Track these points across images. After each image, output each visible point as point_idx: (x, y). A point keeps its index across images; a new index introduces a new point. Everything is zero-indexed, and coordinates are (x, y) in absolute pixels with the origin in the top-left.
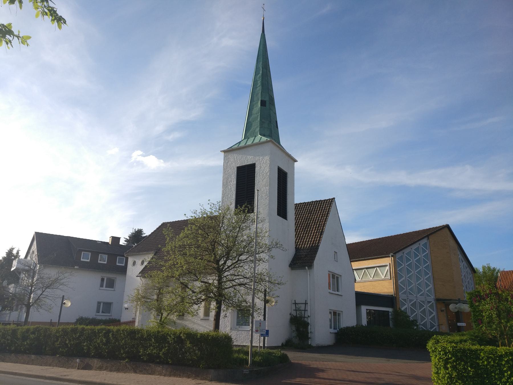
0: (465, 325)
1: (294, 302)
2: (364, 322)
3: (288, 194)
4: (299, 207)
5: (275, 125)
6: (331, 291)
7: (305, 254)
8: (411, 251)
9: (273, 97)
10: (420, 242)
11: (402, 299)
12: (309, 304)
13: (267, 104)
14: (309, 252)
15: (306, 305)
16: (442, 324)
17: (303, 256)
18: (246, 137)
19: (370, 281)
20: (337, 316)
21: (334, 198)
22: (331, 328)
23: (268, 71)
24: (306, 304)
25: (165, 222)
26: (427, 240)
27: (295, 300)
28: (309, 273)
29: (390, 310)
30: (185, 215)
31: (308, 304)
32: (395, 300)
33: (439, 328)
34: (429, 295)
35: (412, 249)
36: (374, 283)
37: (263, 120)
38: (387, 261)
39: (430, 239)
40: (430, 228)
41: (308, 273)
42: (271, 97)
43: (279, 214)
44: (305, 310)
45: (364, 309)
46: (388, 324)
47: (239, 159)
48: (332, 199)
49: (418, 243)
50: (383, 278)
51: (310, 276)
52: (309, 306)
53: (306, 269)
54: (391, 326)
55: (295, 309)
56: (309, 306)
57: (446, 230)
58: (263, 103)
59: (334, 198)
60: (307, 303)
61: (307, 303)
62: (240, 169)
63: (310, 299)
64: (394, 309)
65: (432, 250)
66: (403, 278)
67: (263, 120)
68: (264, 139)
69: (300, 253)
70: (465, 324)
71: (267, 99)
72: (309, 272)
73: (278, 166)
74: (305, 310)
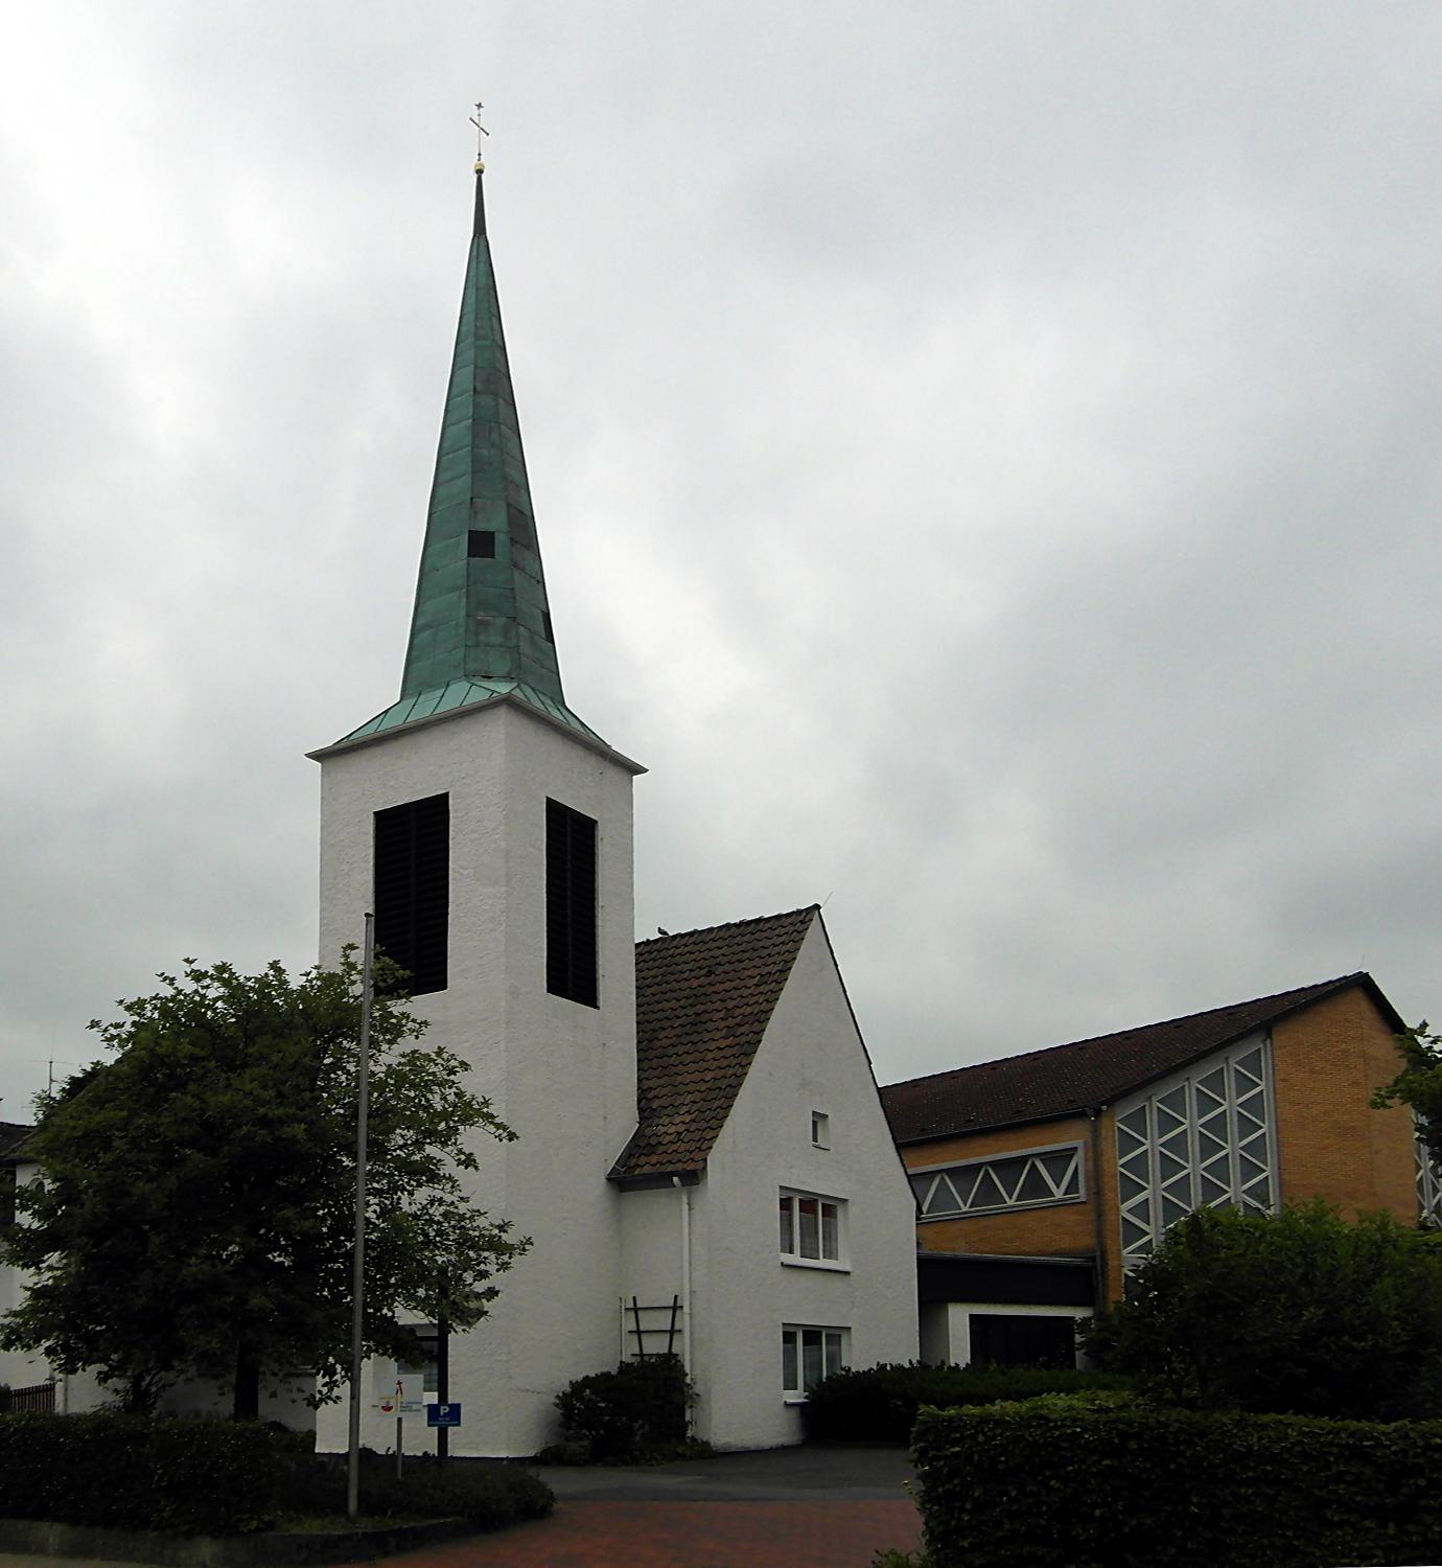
3: (600, 904)
5: (541, 628)
6: (795, 1259)
7: (672, 1129)
8: (1222, 1069)
9: (528, 512)
12: (686, 1309)
15: (678, 1312)
18: (412, 685)
20: (821, 1344)
21: (817, 907)
22: (790, 1384)
23: (501, 401)
24: (676, 1308)
27: (634, 1298)
28: (689, 1198)
29: (1079, 1313)
30: (479, 106)
31: (682, 1307)
32: (1100, 1278)
35: (1188, 1079)
38: (1073, 1137)
39: (1274, 1037)
41: (685, 1200)
44: (672, 1332)
45: (959, 1318)
46: (1070, 1361)
50: (1058, 1194)
51: (690, 1210)
52: (687, 1318)
53: (674, 1186)
54: (1077, 1367)
55: (635, 1329)
56: (687, 1318)
57: (1360, 1003)
60: (679, 1304)
62: (387, 822)
63: (692, 1292)
64: (1095, 1311)
65: (1283, 1080)
74: (672, 1332)
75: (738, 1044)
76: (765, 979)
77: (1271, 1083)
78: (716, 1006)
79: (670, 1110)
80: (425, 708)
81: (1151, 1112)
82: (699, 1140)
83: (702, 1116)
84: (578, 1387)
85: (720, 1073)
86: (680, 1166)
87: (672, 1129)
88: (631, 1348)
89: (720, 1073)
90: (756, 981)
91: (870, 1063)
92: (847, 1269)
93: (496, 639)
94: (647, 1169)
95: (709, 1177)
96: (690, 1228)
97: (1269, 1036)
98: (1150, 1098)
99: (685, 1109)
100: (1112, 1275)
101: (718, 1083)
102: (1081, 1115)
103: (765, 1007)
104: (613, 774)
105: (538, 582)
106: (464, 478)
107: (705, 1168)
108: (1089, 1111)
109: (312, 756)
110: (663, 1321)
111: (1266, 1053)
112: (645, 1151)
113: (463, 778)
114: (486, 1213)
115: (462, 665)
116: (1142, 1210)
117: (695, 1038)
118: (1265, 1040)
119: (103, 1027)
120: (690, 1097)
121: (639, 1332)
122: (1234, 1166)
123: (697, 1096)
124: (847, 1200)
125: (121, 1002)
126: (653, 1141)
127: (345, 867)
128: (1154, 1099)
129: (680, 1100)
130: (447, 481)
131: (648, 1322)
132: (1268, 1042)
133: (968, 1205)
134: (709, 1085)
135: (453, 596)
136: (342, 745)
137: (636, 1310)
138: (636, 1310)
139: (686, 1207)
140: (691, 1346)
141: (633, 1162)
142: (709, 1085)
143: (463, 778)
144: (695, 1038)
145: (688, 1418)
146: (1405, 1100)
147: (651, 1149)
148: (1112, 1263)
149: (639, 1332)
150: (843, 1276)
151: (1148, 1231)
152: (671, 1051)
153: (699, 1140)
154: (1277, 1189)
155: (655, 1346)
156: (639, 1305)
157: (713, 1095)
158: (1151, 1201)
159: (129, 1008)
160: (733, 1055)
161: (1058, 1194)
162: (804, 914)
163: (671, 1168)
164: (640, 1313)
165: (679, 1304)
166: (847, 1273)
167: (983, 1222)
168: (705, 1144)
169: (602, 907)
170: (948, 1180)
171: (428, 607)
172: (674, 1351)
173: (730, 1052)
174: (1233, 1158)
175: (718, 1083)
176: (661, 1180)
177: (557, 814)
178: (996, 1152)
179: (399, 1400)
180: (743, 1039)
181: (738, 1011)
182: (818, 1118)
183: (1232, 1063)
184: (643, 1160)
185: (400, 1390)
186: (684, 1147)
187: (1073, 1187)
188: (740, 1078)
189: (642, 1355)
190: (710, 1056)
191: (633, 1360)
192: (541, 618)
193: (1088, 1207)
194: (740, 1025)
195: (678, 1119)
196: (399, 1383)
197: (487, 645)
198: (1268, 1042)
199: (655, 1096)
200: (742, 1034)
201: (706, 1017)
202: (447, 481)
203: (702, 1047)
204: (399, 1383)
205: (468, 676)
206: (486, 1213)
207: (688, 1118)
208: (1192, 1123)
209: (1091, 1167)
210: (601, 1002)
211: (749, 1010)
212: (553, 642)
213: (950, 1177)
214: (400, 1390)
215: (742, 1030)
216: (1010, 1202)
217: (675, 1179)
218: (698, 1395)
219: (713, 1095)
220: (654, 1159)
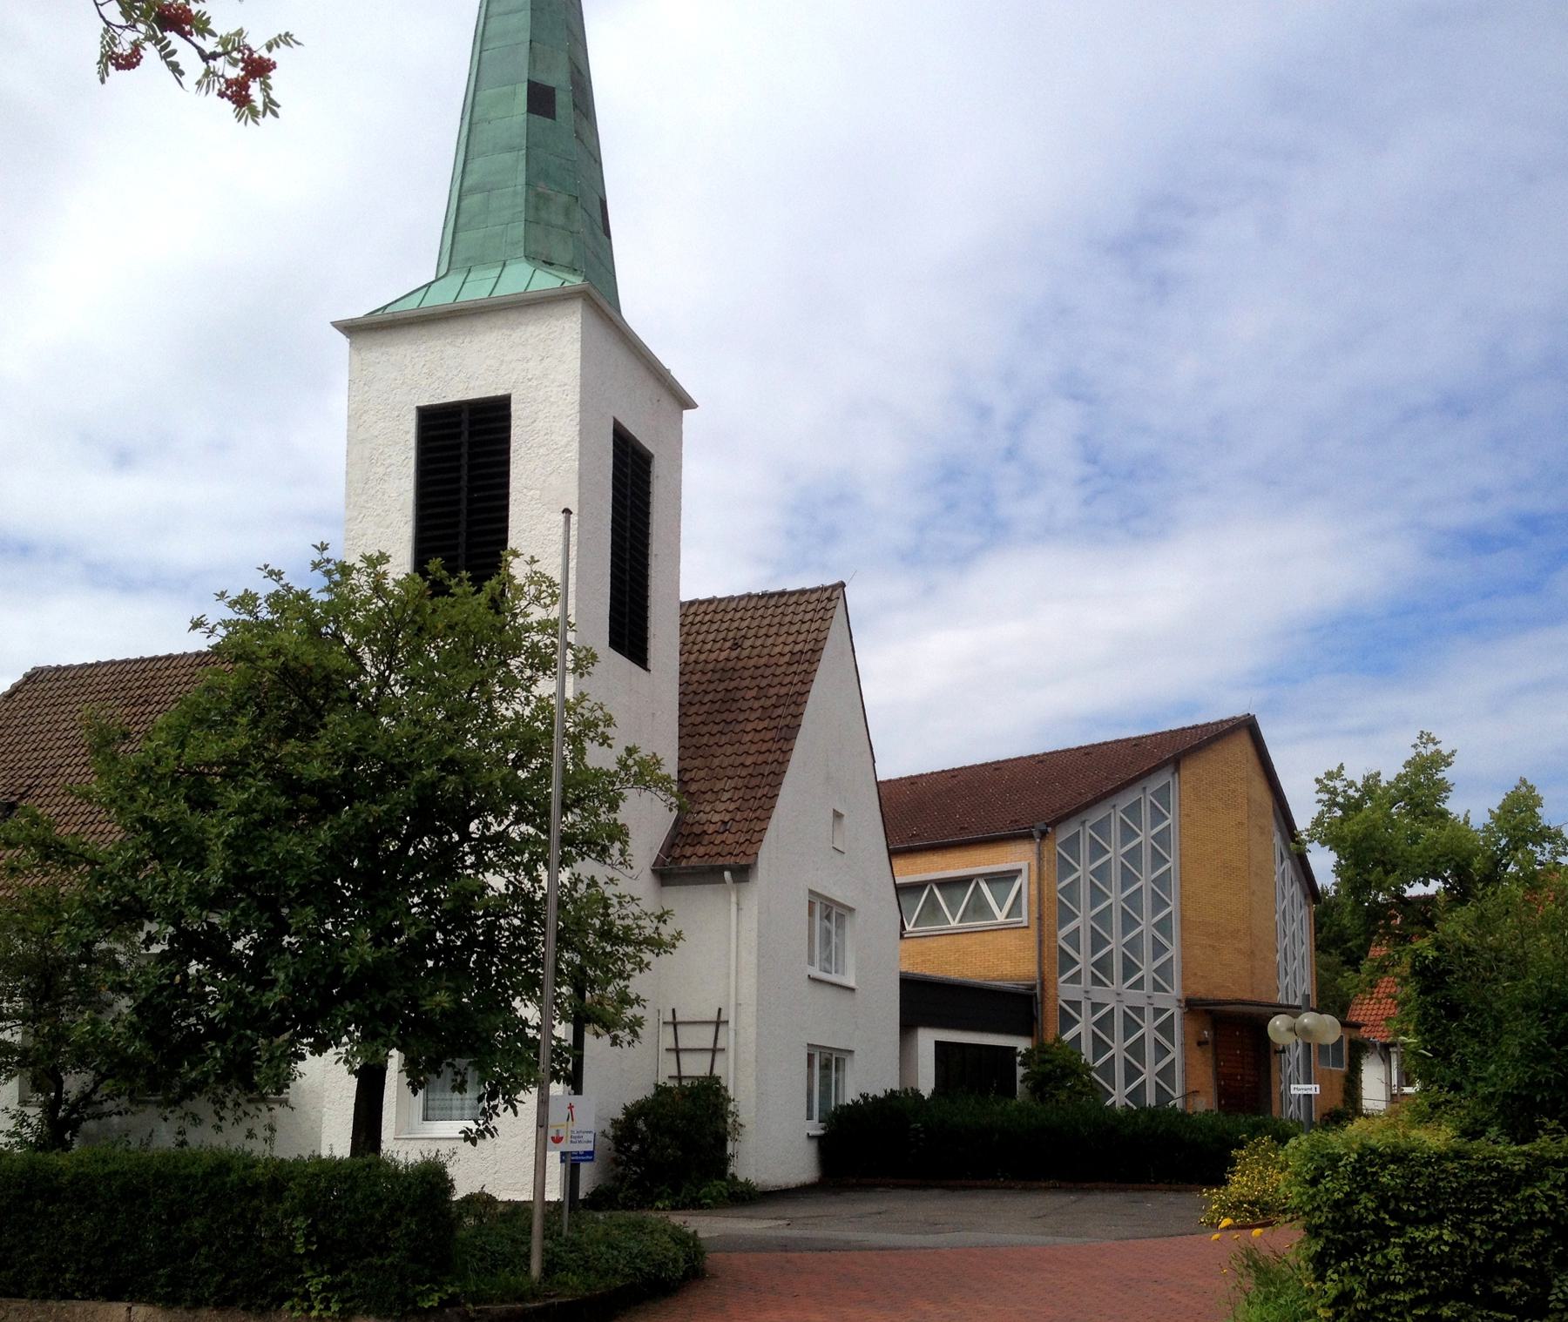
0: (1318, 1092)
1: (669, 1018)
2: (926, 1083)
3: (654, 553)
4: (698, 615)
5: (599, 220)
10: (1144, 783)
11: (1064, 1001)
13: (563, 100)
14: (738, 809)
15: (722, 1028)
16: (1197, 1092)
17: (711, 829)
19: (938, 933)
21: (842, 585)
25: (43, 662)
26: (1173, 774)
27: (674, 1010)
28: (737, 898)
29: (1022, 1044)
32: (1039, 1005)
33: (1186, 1102)
34: (1161, 986)
36: (964, 941)
37: (541, 187)
38: (1018, 857)
39: (1182, 772)
40: (1183, 729)
41: (734, 899)
42: (579, 71)
43: (616, 643)
45: (927, 1040)
47: (425, 370)
48: (834, 587)
49: (1138, 787)
50: (1001, 917)
52: (732, 1034)
53: (724, 882)
55: (673, 1046)
56: (732, 1034)
58: (540, 100)
59: (842, 585)
60: (722, 1019)
61: (722, 1019)
63: (738, 1005)
66: (1074, 919)
67: (541, 187)
68: (546, 281)
69: (698, 813)
70: (1318, 1086)
71: (557, 78)
72: (738, 892)
73: (615, 420)
74: (714, 1051)
75: (775, 727)
76: (797, 658)
77: (1177, 816)
78: (747, 683)
79: (708, 796)
80: (478, 288)
81: (1084, 839)
82: (747, 832)
83: (746, 805)
84: (635, 1112)
85: (761, 758)
86: (730, 860)
87: (716, 818)
88: (668, 1068)
89: (761, 758)
90: (786, 658)
91: (874, 762)
92: (852, 984)
93: (559, 220)
94: (694, 861)
95: (759, 874)
96: (737, 928)
97: (1177, 769)
98: (1083, 823)
99: (726, 796)
100: (1049, 1005)
101: (760, 769)
102: (1028, 837)
103: (799, 687)
104: (667, 403)
105: (596, 161)
106: (523, 12)
107: (755, 863)
108: (1036, 834)
109: (336, 325)
110: (704, 1037)
111: (1174, 787)
112: (689, 841)
113: (530, 380)
114: (639, 899)
115: (522, 244)
116: (1073, 939)
117: (730, 717)
118: (1173, 774)
119: (210, 626)
120: (731, 784)
121: (677, 1051)
122: (1084, 898)
123: (740, 783)
124: (854, 910)
125: (222, 595)
126: (697, 829)
127: (381, 470)
128: (1088, 824)
129: (719, 786)
130: (500, 14)
131: (689, 1037)
132: (1177, 775)
133: (912, 924)
134: (750, 770)
135: (508, 157)
136: (374, 318)
137: (675, 1024)
138: (675, 1024)
139: (734, 908)
140: (735, 1069)
141: (677, 852)
142: (750, 770)
143: (530, 380)
144: (730, 717)
145: (729, 1150)
146: (1323, 844)
147: (697, 838)
148: (1051, 992)
149: (677, 1051)
150: (848, 992)
151: (1077, 959)
152: (704, 729)
153: (747, 832)
154: (1179, 922)
155: (696, 1067)
156: (679, 1018)
157: (754, 782)
158: (1082, 929)
159: (232, 604)
160: (773, 739)
161: (1001, 917)
162: (830, 591)
163: (720, 861)
164: (679, 1028)
165: (723, 1018)
166: (852, 990)
167: (928, 943)
168: (754, 836)
169: (656, 555)
170: (937, 892)
171: (476, 165)
172: (717, 1072)
173: (770, 735)
174: (1146, 889)
175: (760, 769)
176: (709, 874)
177: (623, 441)
178: (942, 869)
179: (570, 1128)
180: (782, 723)
181: (772, 691)
182: (838, 816)
183: (1145, 795)
184: (688, 851)
185: (571, 1117)
186: (730, 838)
187: (1015, 909)
188: (783, 763)
189: (680, 1078)
190: (747, 738)
191: (671, 1084)
192: (598, 203)
193: (1029, 932)
194: (775, 707)
195: (721, 807)
196: (571, 1107)
197: (548, 224)
198: (1177, 775)
199: (692, 779)
200: (780, 716)
201: (739, 695)
202: (500, 14)
203: (738, 728)
204: (571, 1107)
205: (530, 257)
206: (639, 899)
207: (732, 807)
208: (1115, 852)
209: (1034, 892)
210: (651, 664)
211: (783, 691)
212: (609, 236)
213: (939, 889)
214: (571, 1117)
215: (779, 711)
216: (954, 924)
217: (727, 874)
218: (741, 1125)
219: (754, 782)
220: (701, 850)
